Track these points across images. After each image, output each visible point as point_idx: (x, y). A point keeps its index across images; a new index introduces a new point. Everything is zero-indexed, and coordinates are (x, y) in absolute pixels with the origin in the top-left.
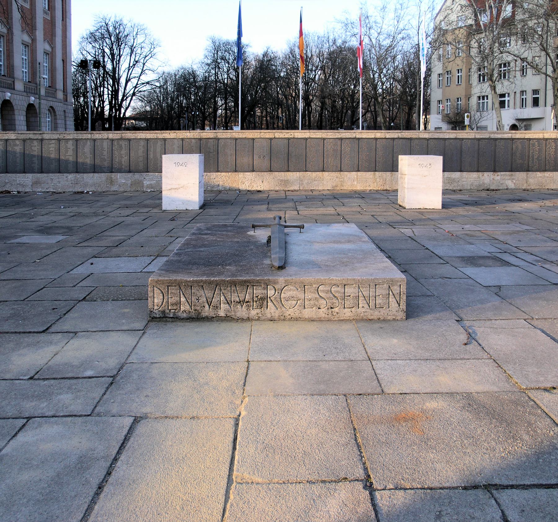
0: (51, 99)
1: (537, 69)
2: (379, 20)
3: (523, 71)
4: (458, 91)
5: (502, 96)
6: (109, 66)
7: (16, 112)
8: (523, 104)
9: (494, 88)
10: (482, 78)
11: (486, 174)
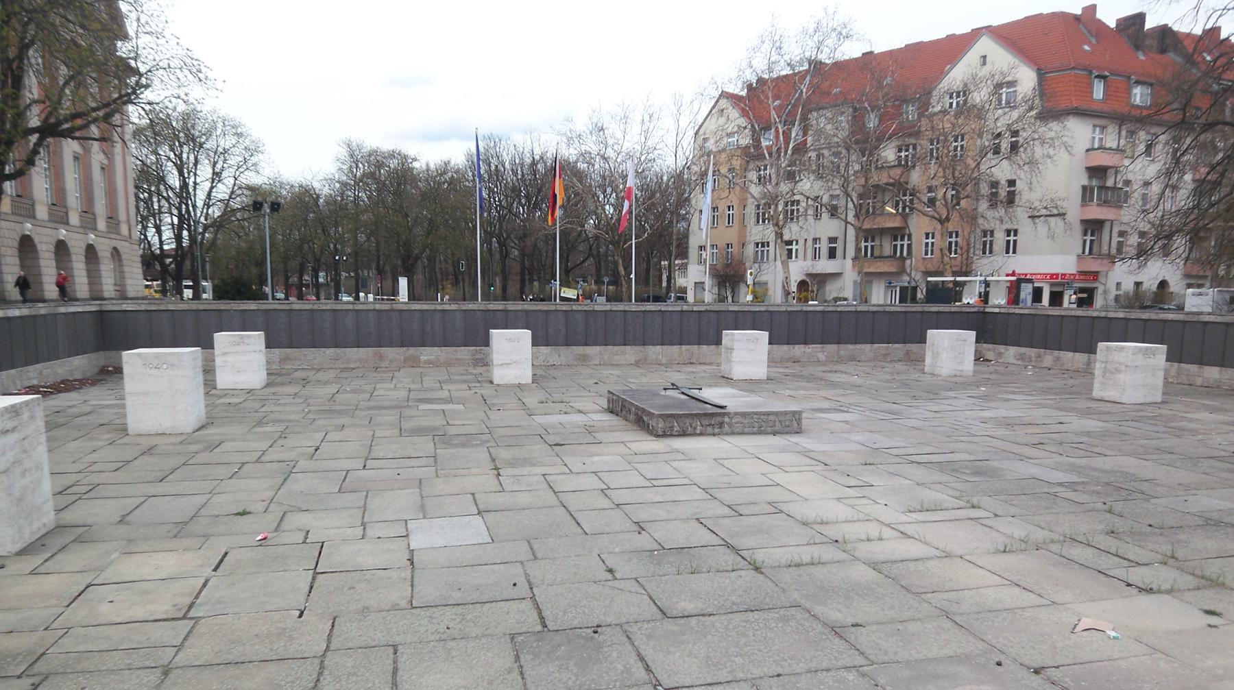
0: (113, 236)
1: (833, 212)
2: (619, 135)
3: (817, 216)
4: (729, 235)
5: (789, 243)
6: (174, 180)
7: (74, 257)
8: (816, 255)
9: (779, 235)
10: (761, 218)
11: (797, 347)
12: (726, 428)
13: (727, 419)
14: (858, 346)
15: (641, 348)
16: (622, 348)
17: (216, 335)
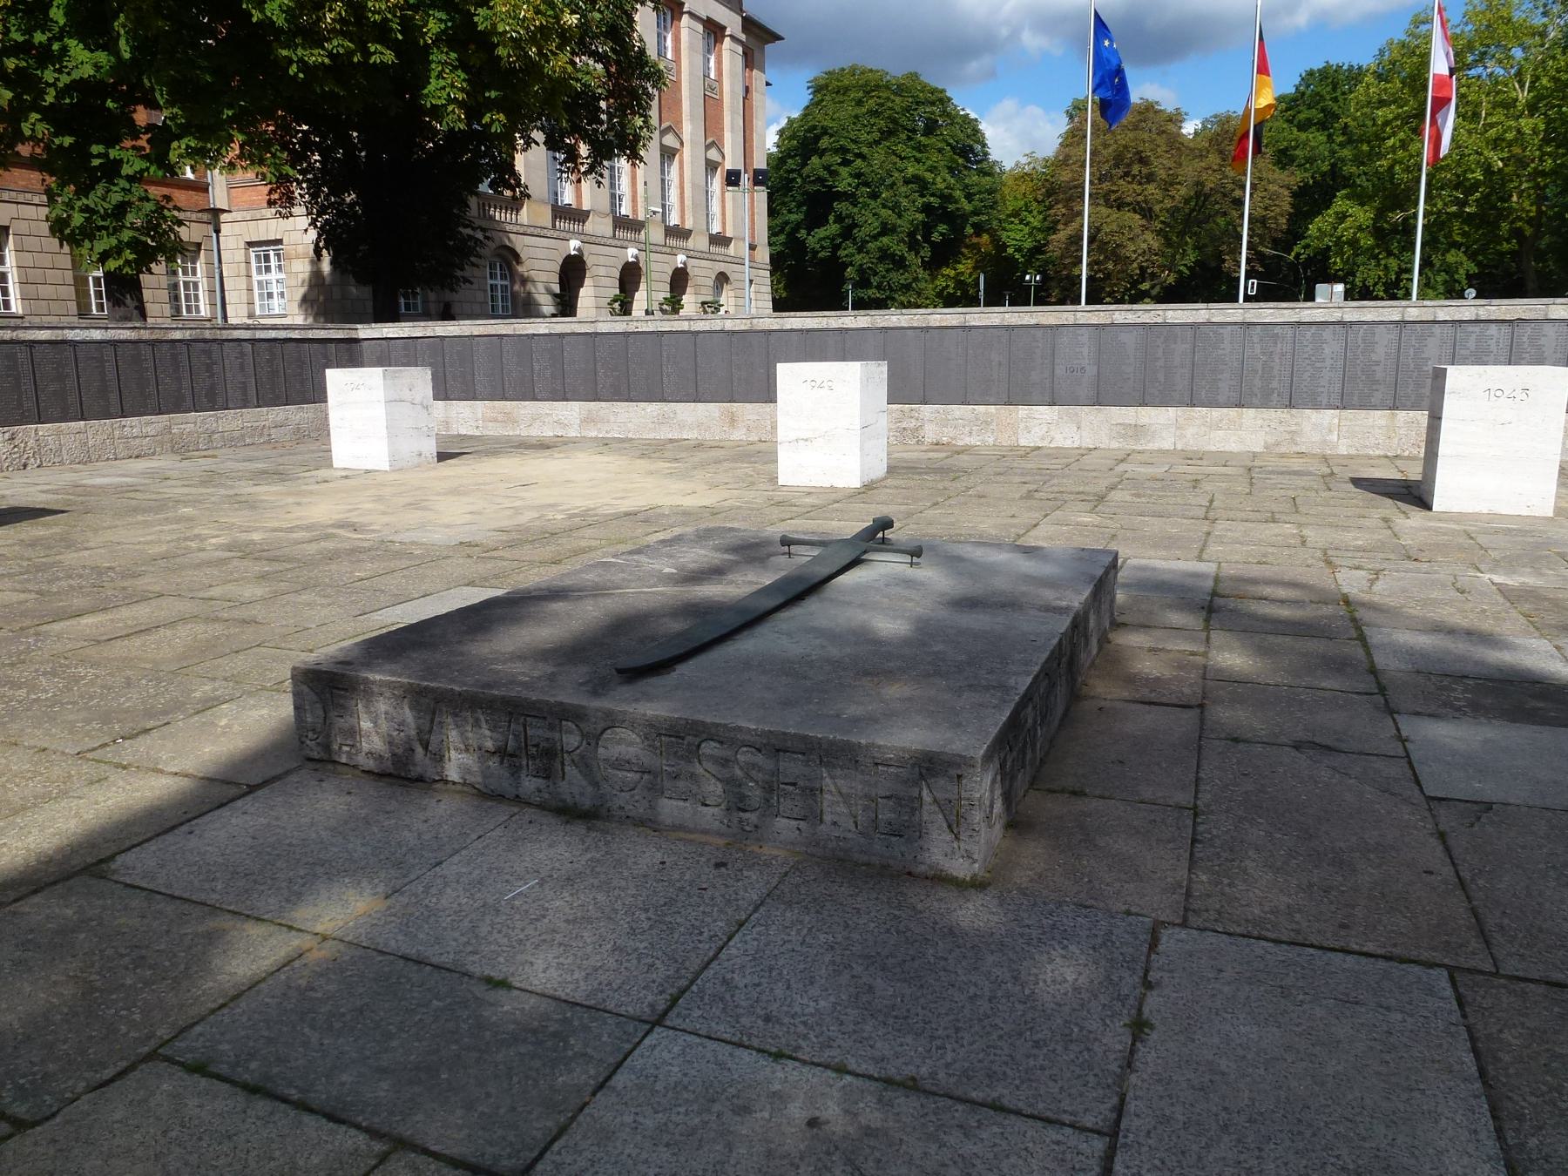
15: (1283, 414)
16: (1233, 412)
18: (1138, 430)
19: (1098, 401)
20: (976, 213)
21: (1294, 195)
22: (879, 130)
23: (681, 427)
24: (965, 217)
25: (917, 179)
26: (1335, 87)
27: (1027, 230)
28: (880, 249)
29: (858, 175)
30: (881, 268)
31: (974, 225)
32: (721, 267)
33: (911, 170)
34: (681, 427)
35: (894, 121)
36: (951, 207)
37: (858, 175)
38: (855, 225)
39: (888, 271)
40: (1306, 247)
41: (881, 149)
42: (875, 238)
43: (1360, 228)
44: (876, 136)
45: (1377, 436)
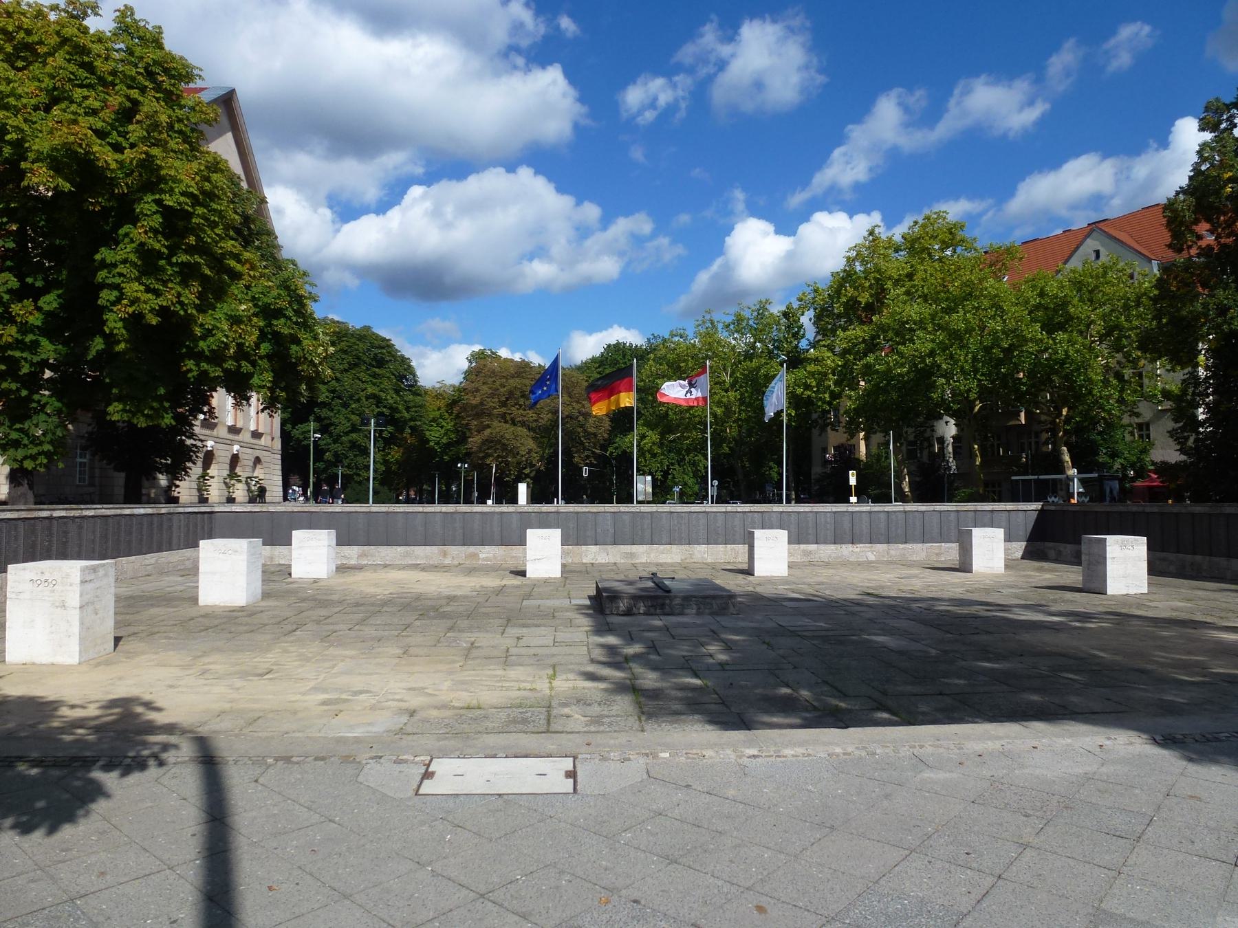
12: (667, 609)
13: (667, 601)
14: (908, 546)
15: (687, 547)
16: (668, 547)
17: (294, 532)
18: (632, 555)
19: (615, 544)
20: (412, 419)
21: (612, 420)
22: (349, 363)
23: (417, 558)
24: (405, 422)
25: (374, 396)
26: (624, 356)
27: (443, 431)
28: (350, 441)
29: (333, 391)
30: (350, 454)
31: (411, 428)
32: (258, 453)
33: (370, 390)
34: (417, 558)
35: (359, 358)
36: (397, 416)
37: (333, 391)
38: (332, 424)
39: (355, 456)
40: (616, 448)
41: (349, 375)
42: (347, 434)
43: (654, 443)
44: (346, 366)
45: (734, 554)
